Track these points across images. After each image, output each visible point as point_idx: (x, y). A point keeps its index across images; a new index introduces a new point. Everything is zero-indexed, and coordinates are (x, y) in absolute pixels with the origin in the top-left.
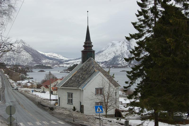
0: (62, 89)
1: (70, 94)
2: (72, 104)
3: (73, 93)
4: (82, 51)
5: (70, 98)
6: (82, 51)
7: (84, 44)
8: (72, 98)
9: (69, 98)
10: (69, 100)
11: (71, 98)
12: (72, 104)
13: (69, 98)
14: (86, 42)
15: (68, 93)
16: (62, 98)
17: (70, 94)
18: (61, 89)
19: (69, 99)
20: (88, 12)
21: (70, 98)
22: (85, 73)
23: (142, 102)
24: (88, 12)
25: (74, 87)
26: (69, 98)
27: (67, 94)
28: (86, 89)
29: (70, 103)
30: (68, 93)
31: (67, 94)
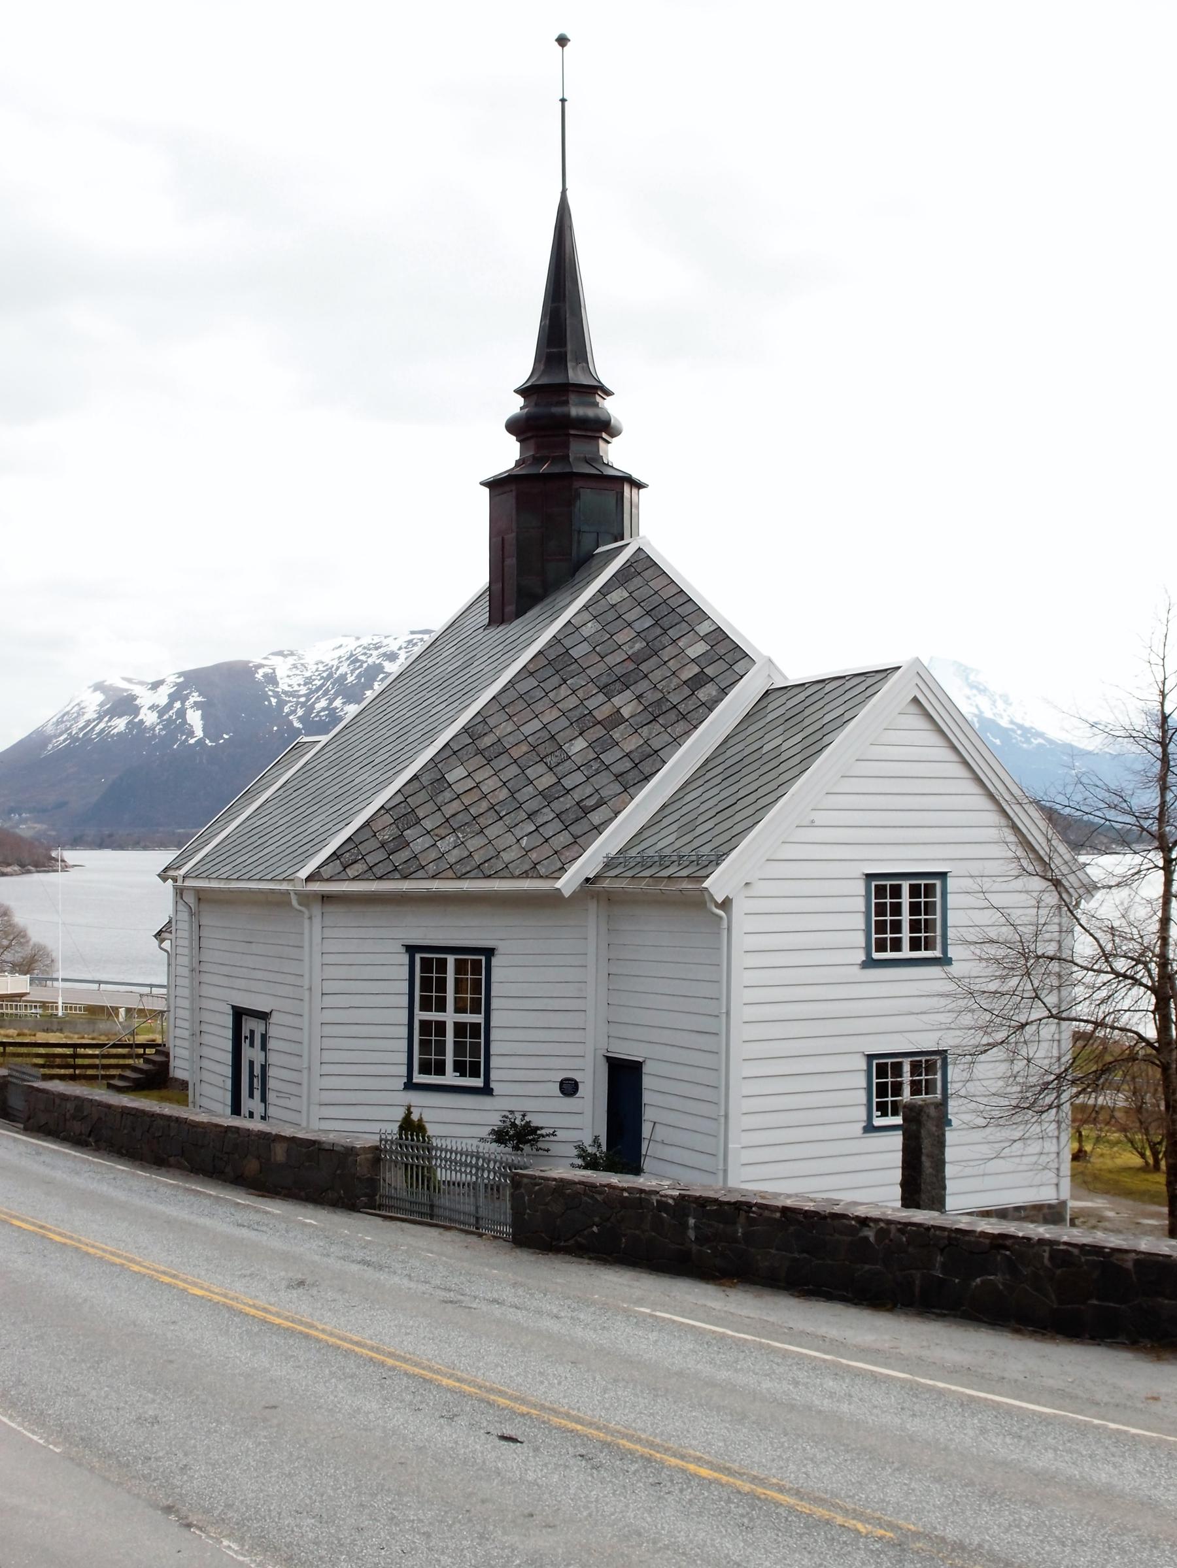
0: (326, 899)
1: (451, 960)
2: (487, 1090)
3: (489, 952)
4: (495, 485)
5: (442, 1008)
6: (495, 485)
7: (520, 401)
8: (479, 1019)
9: (468, 1018)
10: (424, 1044)
11: (441, 1026)
12: (487, 1090)
13: (426, 1006)
14: (545, 381)
15: (411, 950)
16: (328, 1016)
17: (451, 960)
18: (306, 899)
19: (425, 1025)
20: (562, 41)
21: (442, 1008)
22: (626, 704)
23: (718, 1424)
24: (562, 41)
25: (525, 875)
26: (468, 1018)
27: (398, 968)
28: (761, 888)
29: (440, 1070)
30: (411, 950)
31: (405, 959)
